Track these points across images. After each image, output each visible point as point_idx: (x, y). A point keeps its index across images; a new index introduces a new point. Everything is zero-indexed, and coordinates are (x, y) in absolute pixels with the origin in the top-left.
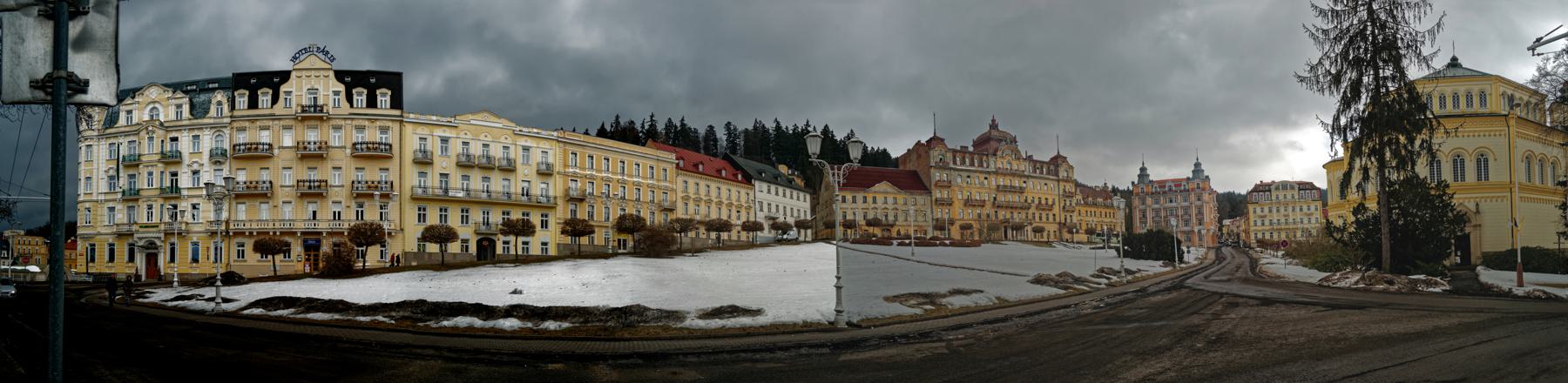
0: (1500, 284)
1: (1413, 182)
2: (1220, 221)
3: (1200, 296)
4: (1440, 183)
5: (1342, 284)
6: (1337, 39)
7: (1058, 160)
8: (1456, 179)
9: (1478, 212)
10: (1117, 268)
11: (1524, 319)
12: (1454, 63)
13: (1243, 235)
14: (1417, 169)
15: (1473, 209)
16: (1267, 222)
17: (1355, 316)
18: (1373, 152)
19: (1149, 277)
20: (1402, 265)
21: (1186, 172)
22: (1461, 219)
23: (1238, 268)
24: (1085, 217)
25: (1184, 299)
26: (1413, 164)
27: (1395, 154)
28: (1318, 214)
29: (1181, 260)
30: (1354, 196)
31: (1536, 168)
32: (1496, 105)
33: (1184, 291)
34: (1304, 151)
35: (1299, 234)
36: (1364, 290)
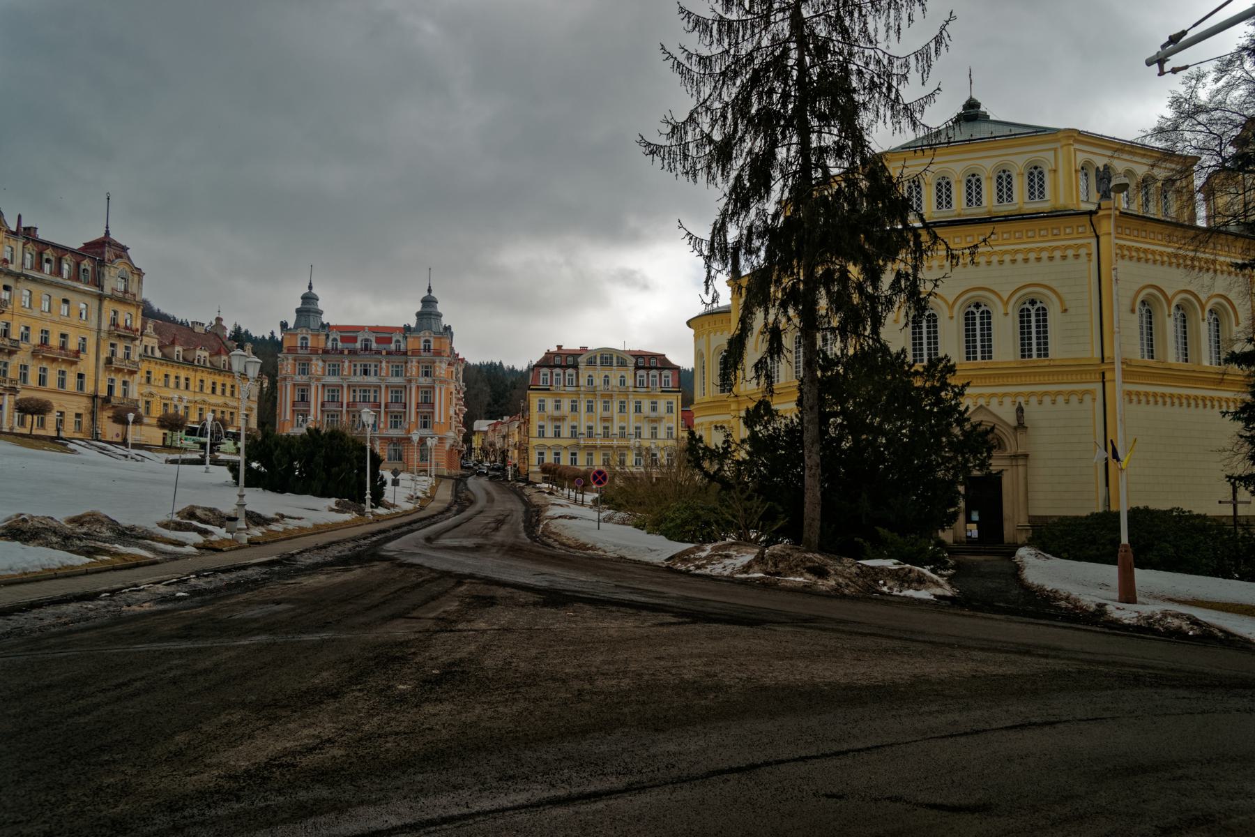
0: (1075, 592)
1: (876, 361)
2: (468, 421)
3: (413, 578)
4: (933, 363)
5: (716, 569)
6: (728, 75)
7: (101, 252)
8: (970, 355)
9: (1021, 426)
10: (228, 508)
11: (1137, 681)
12: (971, 113)
13: (514, 455)
14: (884, 333)
15: (1011, 419)
16: (566, 431)
17: (742, 640)
18: (792, 297)
19: (302, 533)
20: (845, 539)
21: (403, 313)
22: (982, 440)
23: (500, 522)
24: (162, 388)
25: (376, 581)
26: (877, 322)
27: (839, 302)
28: (673, 421)
29: (378, 499)
30: (748, 386)
31: (1169, 326)
32: (1070, 189)
33: (379, 566)
34: (652, 290)
35: (631, 459)
36: (763, 585)
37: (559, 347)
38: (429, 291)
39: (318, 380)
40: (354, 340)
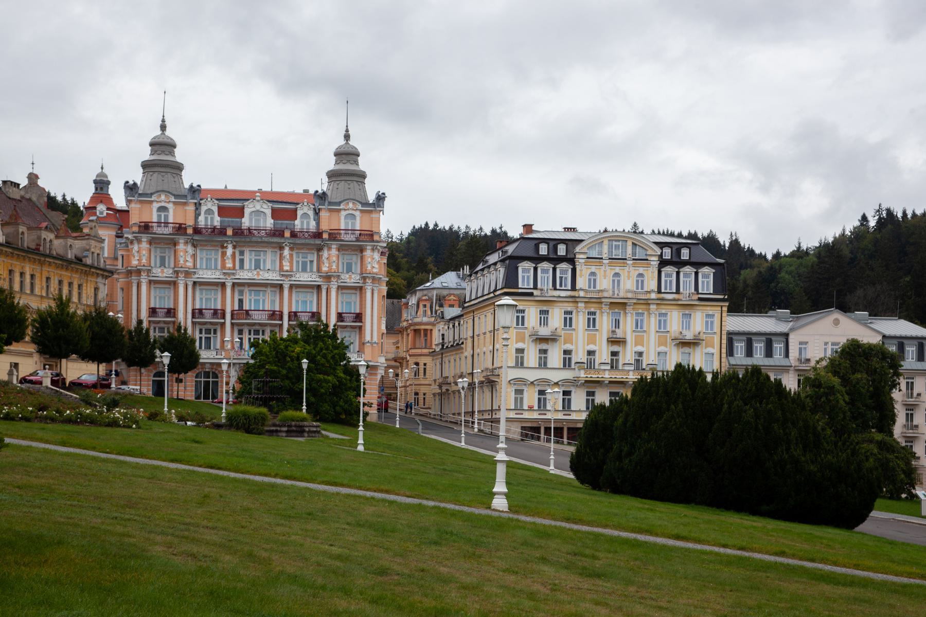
38: (347, 137)
39: (188, 274)
40: (240, 212)
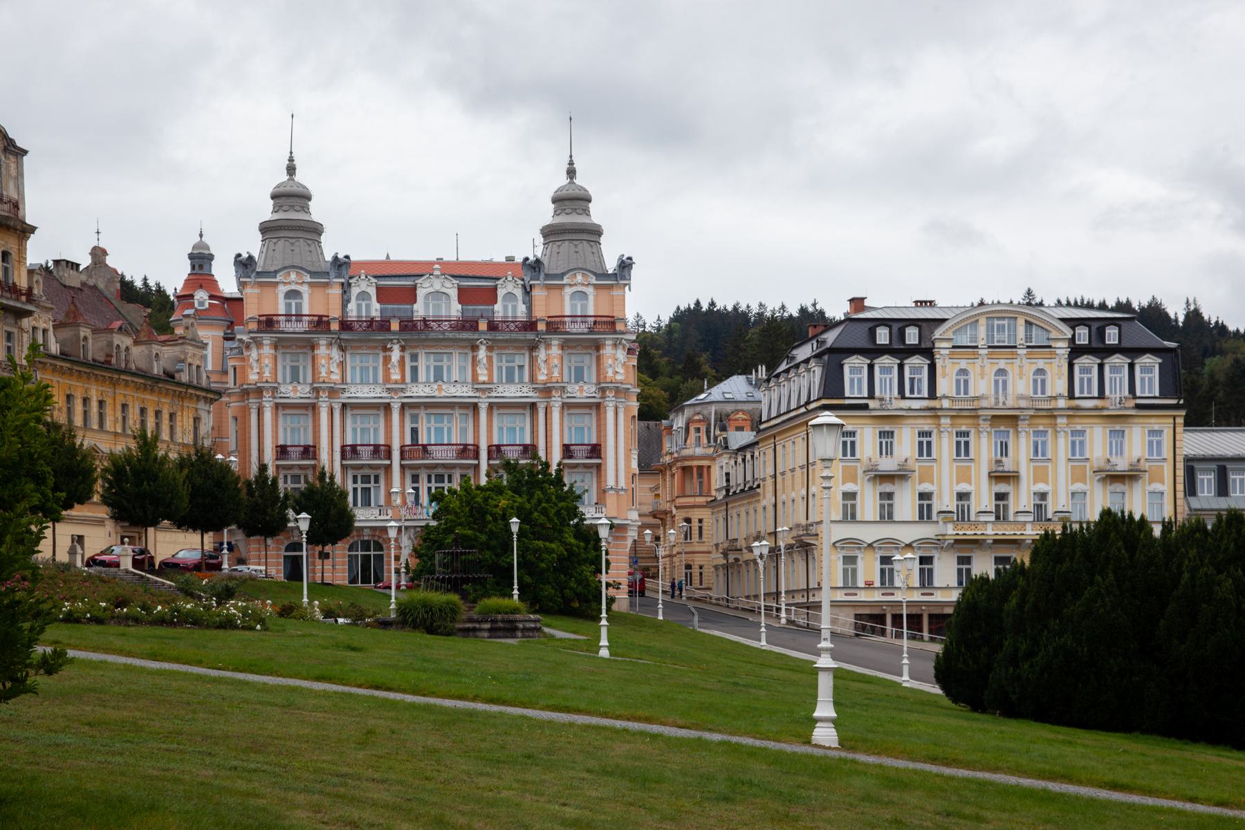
16: (906, 505)
37: (291, 220)
39: (333, 392)
